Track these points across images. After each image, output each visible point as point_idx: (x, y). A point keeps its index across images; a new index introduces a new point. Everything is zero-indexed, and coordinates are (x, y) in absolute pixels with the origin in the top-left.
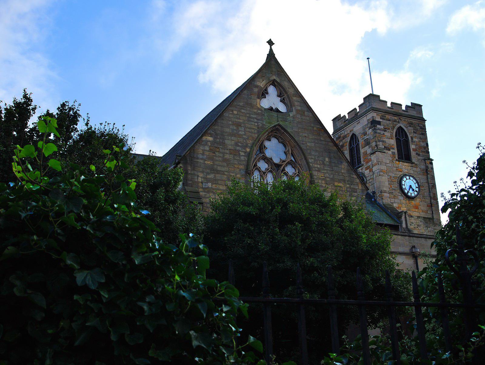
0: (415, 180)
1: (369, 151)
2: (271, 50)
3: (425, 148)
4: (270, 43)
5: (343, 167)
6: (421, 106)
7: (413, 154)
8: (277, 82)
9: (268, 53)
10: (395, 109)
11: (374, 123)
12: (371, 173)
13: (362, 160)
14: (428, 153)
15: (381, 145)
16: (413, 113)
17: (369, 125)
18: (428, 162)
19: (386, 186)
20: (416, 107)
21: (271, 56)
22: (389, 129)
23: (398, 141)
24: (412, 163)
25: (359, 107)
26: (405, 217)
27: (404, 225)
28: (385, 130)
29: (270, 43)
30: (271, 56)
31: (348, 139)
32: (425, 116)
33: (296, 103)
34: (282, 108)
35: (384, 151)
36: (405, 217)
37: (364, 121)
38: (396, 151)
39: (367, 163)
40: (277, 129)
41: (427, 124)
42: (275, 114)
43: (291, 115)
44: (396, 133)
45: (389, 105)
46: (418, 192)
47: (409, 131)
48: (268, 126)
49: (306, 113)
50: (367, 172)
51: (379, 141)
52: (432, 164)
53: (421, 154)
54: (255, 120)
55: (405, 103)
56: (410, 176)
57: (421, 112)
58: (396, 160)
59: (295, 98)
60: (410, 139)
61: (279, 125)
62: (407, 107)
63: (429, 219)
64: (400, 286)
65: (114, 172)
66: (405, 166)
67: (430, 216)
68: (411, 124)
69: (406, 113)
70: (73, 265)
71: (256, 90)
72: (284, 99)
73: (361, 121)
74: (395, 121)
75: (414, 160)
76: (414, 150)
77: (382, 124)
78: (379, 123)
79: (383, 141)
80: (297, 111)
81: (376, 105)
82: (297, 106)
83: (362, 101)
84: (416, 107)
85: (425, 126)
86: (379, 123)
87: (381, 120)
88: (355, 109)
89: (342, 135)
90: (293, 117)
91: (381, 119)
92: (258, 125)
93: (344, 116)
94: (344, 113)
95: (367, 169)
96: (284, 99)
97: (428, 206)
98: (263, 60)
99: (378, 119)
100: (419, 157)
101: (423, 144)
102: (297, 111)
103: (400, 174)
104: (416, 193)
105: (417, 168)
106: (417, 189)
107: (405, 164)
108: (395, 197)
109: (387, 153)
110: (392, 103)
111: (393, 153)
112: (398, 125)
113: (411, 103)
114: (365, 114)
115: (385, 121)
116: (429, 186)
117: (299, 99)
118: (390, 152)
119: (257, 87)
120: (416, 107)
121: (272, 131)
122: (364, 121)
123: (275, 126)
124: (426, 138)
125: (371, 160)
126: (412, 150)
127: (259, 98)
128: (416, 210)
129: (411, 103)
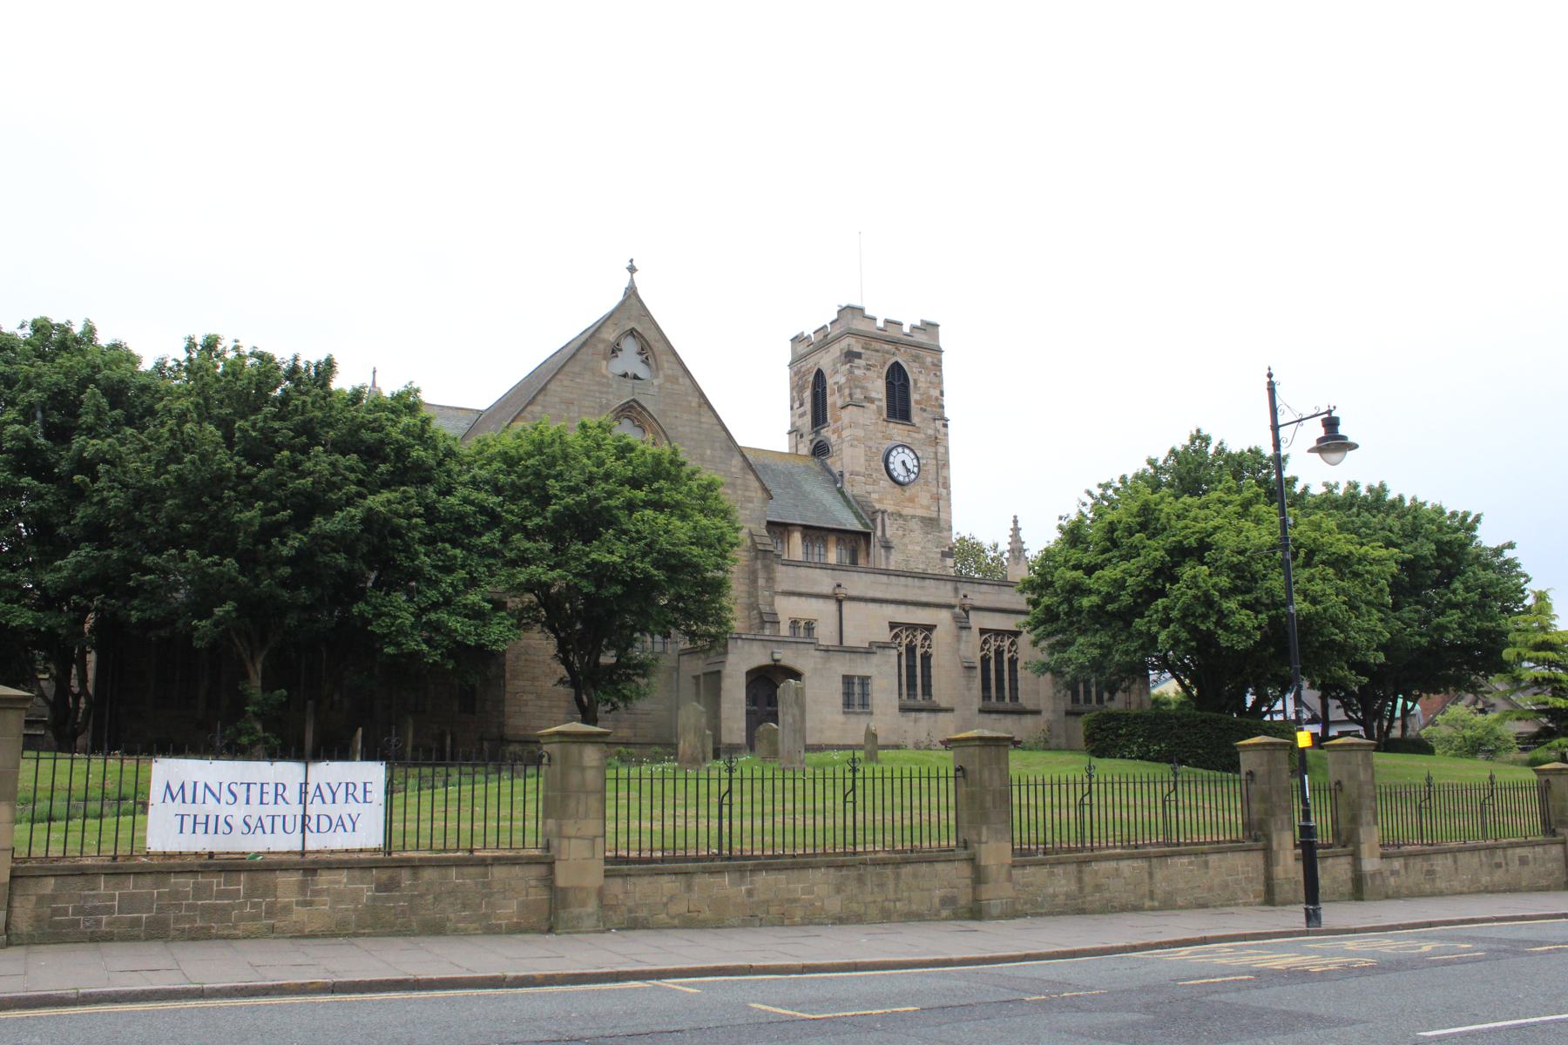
0: (915, 453)
1: (839, 403)
2: (632, 280)
3: (937, 399)
4: (632, 269)
5: (734, 462)
7: (914, 408)
8: (637, 332)
9: (627, 286)
10: (892, 332)
12: (840, 441)
13: (828, 416)
14: (942, 407)
15: (858, 395)
16: (920, 338)
17: (843, 358)
18: (939, 424)
20: (929, 329)
21: (631, 293)
22: (875, 366)
24: (913, 425)
25: (831, 323)
26: (883, 520)
27: (879, 533)
29: (632, 269)
30: (631, 293)
31: (811, 379)
32: (942, 345)
33: (666, 365)
34: (642, 371)
35: (863, 404)
36: (883, 520)
37: (836, 350)
38: (884, 404)
39: (836, 421)
40: (632, 407)
41: (945, 357)
43: (656, 382)
44: (888, 372)
45: (880, 324)
46: (918, 475)
49: (681, 380)
50: (833, 438)
51: (857, 387)
52: (945, 426)
53: (929, 409)
54: (597, 395)
56: (904, 446)
57: (936, 336)
58: (884, 420)
59: (664, 357)
60: (911, 382)
61: (634, 400)
62: (914, 328)
63: (930, 519)
64: (496, 642)
66: (897, 431)
67: (934, 515)
68: (916, 358)
69: (910, 338)
70: (407, 993)
71: (601, 347)
72: (647, 358)
73: (831, 349)
74: (888, 352)
75: (915, 419)
76: (917, 402)
77: (863, 356)
78: (859, 355)
79: (862, 388)
82: (667, 365)
84: (930, 327)
85: (940, 361)
86: (859, 355)
87: (862, 351)
88: (825, 326)
89: (803, 370)
90: (660, 387)
91: (863, 348)
92: (601, 402)
93: (809, 336)
94: (809, 331)
95: (834, 432)
96: (647, 358)
97: (931, 498)
99: (857, 348)
100: (925, 415)
101: (935, 393)
103: (888, 444)
104: (913, 476)
105: (919, 432)
106: (916, 470)
107: (900, 426)
108: (875, 482)
109: (868, 408)
110: (887, 322)
111: (879, 408)
112: (893, 360)
113: (922, 321)
114: (837, 339)
115: (869, 352)
116: (937, 465)
117: (672, 359)
118: (873, 407)
119: (603, 341)
120: (930, 327)
121: (622, 410)
122: (836, 350)
123: (628, 402)
124: (941, 383)
125: (840, 419)
126: (913, 404)
127: (605, 359)
128: (911, 505)
129: (922, 321)
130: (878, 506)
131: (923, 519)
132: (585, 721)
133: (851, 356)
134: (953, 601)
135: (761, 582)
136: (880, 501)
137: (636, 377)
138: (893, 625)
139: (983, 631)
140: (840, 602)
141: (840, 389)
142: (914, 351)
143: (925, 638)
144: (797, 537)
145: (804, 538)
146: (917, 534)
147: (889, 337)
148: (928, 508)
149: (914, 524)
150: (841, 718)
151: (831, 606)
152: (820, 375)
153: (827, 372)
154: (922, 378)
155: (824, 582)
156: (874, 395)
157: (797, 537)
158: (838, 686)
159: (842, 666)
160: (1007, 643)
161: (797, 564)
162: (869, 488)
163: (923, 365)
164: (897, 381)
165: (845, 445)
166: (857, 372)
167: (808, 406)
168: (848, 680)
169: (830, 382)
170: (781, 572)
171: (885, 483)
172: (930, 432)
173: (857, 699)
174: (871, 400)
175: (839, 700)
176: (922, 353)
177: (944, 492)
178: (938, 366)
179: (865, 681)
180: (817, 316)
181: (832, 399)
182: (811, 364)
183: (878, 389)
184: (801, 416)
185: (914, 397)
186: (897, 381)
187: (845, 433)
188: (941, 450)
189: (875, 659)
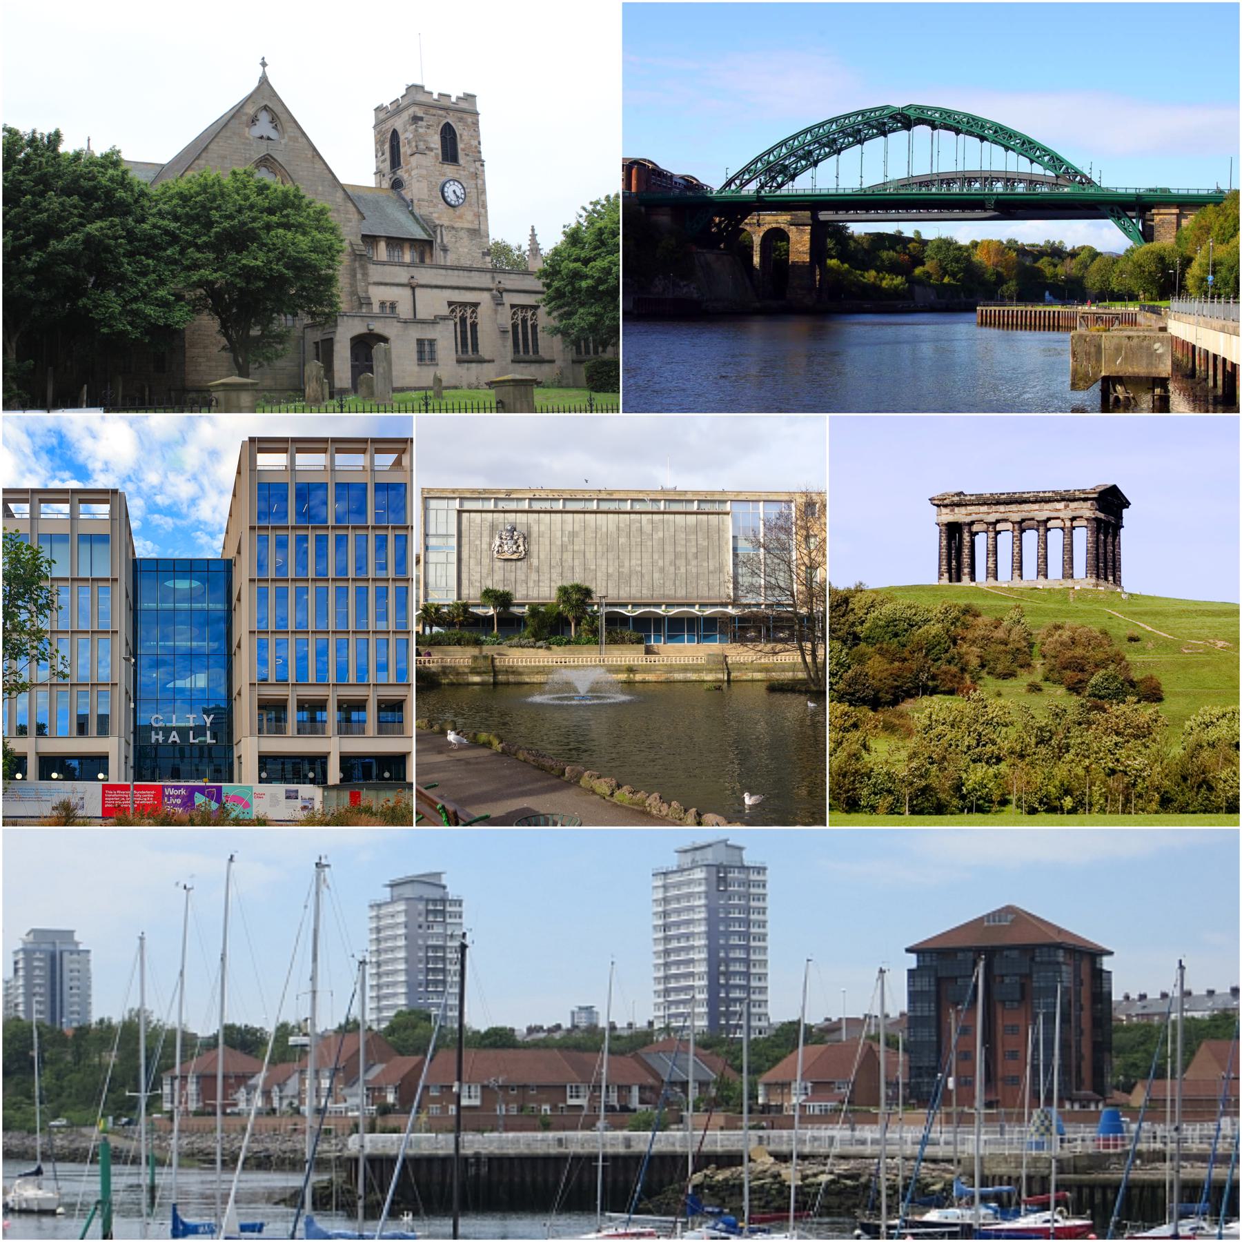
1: (409, 152)
4: (264, 64)
6: (474, 96)
10: (444, 102)
11: (416, 119)
16: (463, 105)
18: (478, 164)
19: (424, 194)
21: (264, 81)
23: (443, 139)
27: (439, 240)
28: (428, 127)
30: (264, 81)
31: (389, 136)
34: (273, 134)
37: (406, 116)
38: (440, 152)
41: (481, 118)
42: (265, 142)
47: (458, 128)
48: (256, 157)
55: (455, 93)
57: (474, 104)
62: (459, 98)
65: (272, 311)
66: (449, 170)
68: (461, 120)
71: (244, 118)
75: (461, 161)
78: (421, 119)
80: (290, 138)
81: (421, 98)
83: (404, 92)
86: (421, 119)
98: (255, 84)
99: (420, 114)
102: (290, 138)
103: (444, 179)
108: (435, 206)
110: (440, 95)
111: (437, 155)
114: (407, 107)
118: (432, 154)
120: (470, 98)
122: (406, 116)
124: (478, 136)
130: (437, 222)
131: (469, 230)
132: (241, 375)
133: (416, 119)
134: (491, 286)
135: (359, 276)
136: (439, 218)
137: (269, 139)
138: (450, 304)
139: (512, 306)
140: (413, 288)
141: (409, 142)
142: (459, 115)
143: (473, 312)
144: (382, 245)
145: (387, 245)
146: (466, 241)
147: (442, 105)
148: (472, 222)
149: (463, 234)
150: (416, 368)
151: (408, 291)
152: (395, 134)
153: (400, 131)
154: (465, 133)
155: (402, 275)
156: (432, 146)
157: (382, 245)
158: (413, 347)
159: (416, 333)
160: (530, 314)
161: (383, 263)
162: (431, 210)
163: (465, 124)
164: (448, 134)
165: (414, 180)
166: (421, 130)
167: (387, 155)
168: (420, 342)
169: (402, 138)
170: (372, 269)
171: (442, 205)
172: (472, 170)
173: (427, 355)
174: (431, 149)
175: (415, 356)
176: (465, 116)
177: (482, 211)
178: (476, 124)
179: (432, 342)
180: (392, 93)
181: (405, 150)
182: (389, 126)
183: (435, 141)
184: (384, 161)
185: (460, 146)
186: (448, 134)
187: (413, 173)
188: (480, 182)
189: (439, 327)
